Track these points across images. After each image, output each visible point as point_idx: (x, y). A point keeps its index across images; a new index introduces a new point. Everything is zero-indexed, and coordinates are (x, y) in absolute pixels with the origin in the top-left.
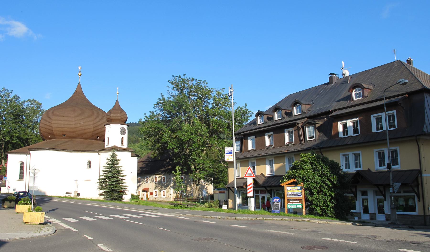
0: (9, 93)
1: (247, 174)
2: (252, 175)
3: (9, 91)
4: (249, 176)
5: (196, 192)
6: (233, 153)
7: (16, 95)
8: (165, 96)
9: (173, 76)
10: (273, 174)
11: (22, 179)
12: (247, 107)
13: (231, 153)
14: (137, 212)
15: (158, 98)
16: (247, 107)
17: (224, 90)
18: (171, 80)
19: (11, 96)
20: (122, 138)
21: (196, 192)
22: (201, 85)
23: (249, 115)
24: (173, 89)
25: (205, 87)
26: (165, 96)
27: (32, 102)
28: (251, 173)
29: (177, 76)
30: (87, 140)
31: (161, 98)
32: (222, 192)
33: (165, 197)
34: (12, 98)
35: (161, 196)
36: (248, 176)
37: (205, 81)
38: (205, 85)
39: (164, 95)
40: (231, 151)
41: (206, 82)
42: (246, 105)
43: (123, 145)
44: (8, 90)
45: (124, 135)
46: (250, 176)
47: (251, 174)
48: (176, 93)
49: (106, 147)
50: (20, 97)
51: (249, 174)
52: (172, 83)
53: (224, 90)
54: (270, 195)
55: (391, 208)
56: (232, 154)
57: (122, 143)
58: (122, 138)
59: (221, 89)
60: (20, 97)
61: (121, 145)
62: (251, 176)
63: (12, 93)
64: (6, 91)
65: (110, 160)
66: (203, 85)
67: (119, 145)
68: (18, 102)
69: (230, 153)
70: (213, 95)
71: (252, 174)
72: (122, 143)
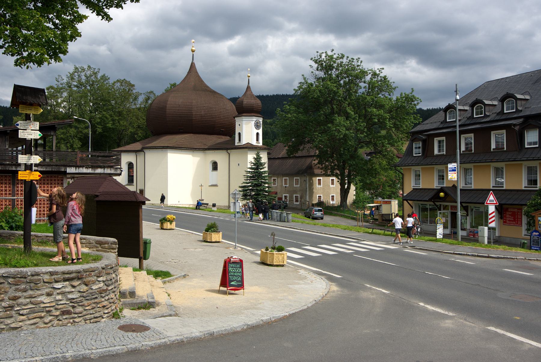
0: (96, 73)
1: (489, 201)
2: (495, 202)
3: (96, 70)
4: (491, 202)
5: (344, 200)
6: (457, 171)
7: (104, 75)
8: (308, 79)
9: (318, 52)
10: (472, 187)
11: (132, 184)
12: (413, 94)
13: (455, 170)
14: (414, 253)
15: (299, 82)
16: (413, 94)
17: (383, 71)
18: (315, 58)
19: (99, 76)
20: (258, 134)
21: (344, 200)
22: (353, 63)
23: (416, 102)
24: (317, 69)
25: (358, 66)
26: (308, 79)
27: (123, 82)
28: (493, 199)
29: (323, 53)
30: (203, 136)
31: (303, 81)
32: (386, 203)
33: (298, 203)
34: (99, 78)
35: (293, 203)
36: (490, 202)
37: (359, 58)
38: (359, 64)
39: (307, 78)
40: (455, 168)
41: (360, 60)
42: (413, 91)
43: (258, 142)
44: (95, 69)
45: (259, 129)
46: (492, 202)
47: (492, 201)
48: (321, 74)
49: (236, 144)
50: (109, 78)
51: (491, 201)
52: (316, 62)
53: (383, 71)
54: (465, 212)
55: (415, 175)
56: (456, 172)
57: (257, 140)
58: (258, 134)
59: (378, 69)
60: (109, 78)
61: (256, 142)
62: (493, 202)
63: (99, 72)
64: (92, 70)
65: (253, 163)
66: (355, 63)
67: (254, 143)
68: (107, 84)
69: (453, 170)
70: (368, 78)
71: (494, 201)
72: (257, 140)
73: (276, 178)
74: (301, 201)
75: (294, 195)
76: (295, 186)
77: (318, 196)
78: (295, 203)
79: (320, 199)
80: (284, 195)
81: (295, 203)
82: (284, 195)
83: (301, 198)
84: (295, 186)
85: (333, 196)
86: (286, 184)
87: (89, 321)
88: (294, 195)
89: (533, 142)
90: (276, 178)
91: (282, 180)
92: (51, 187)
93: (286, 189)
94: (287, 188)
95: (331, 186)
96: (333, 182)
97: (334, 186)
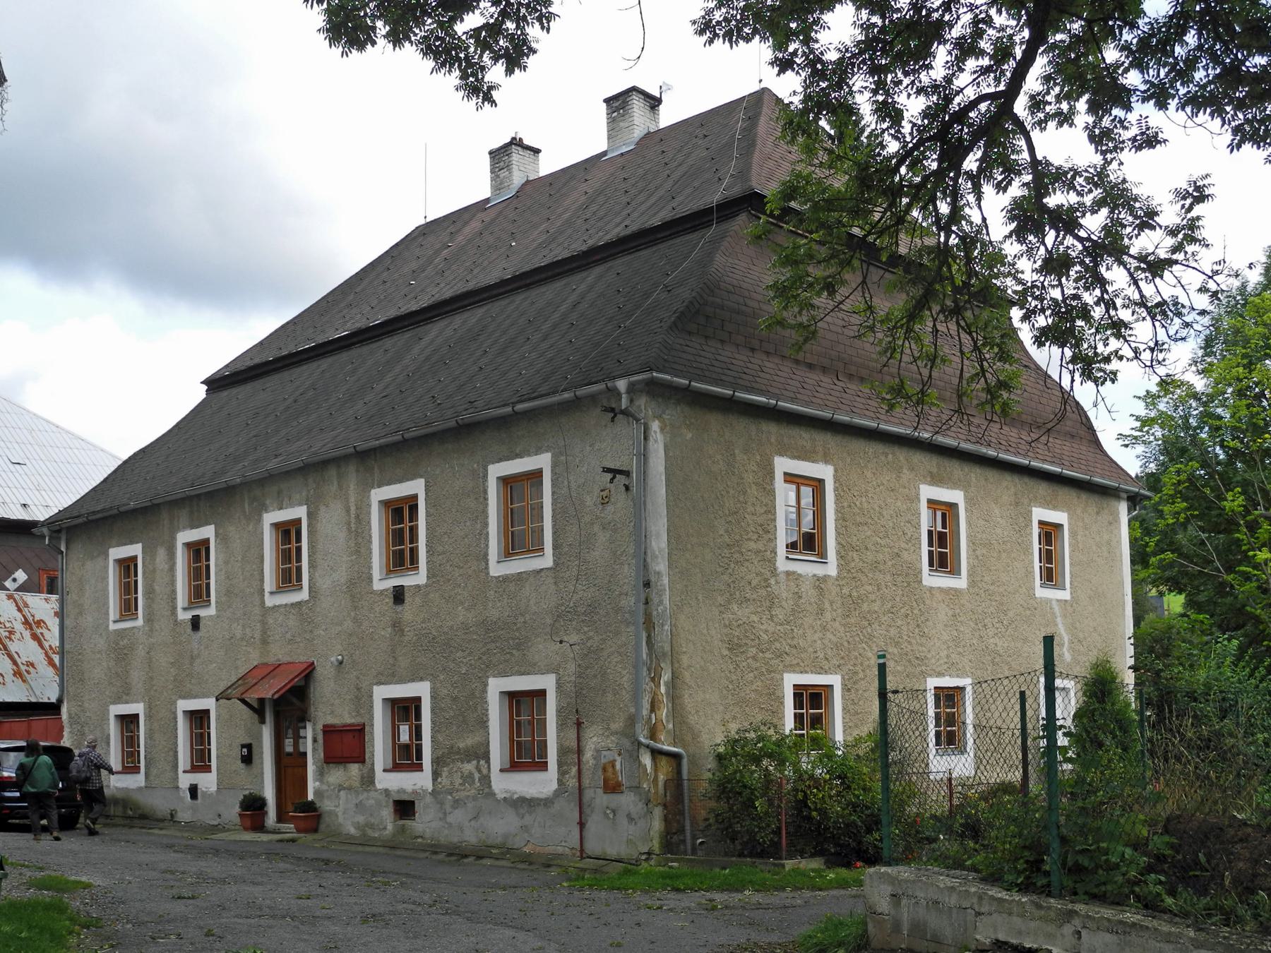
35: (486, 779)
73: (300, 512)
74: (572, 754)
75: (496, 686)
76: (497, 569)
77: (799, 691)
78: (506, 784)
79: (816, 721)
80: (382, 692)
81: (506, 784)
82: (382, 692)
83: (575, 720)
84: (497, 569)
85: (949, 697)
86: (401, 559)
87: (574, 744)
88: (496, 686)
89: (795, 709)
90: (300, 512)
91: (363, 508)
92: (1051, 809)
93: (397, 626)
94: (408, 612)
95: (934, 581)
96: (942, 538)
97: (961, 583)
